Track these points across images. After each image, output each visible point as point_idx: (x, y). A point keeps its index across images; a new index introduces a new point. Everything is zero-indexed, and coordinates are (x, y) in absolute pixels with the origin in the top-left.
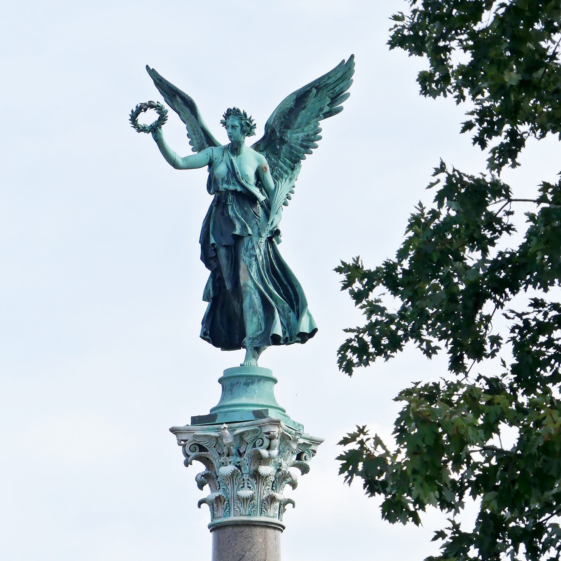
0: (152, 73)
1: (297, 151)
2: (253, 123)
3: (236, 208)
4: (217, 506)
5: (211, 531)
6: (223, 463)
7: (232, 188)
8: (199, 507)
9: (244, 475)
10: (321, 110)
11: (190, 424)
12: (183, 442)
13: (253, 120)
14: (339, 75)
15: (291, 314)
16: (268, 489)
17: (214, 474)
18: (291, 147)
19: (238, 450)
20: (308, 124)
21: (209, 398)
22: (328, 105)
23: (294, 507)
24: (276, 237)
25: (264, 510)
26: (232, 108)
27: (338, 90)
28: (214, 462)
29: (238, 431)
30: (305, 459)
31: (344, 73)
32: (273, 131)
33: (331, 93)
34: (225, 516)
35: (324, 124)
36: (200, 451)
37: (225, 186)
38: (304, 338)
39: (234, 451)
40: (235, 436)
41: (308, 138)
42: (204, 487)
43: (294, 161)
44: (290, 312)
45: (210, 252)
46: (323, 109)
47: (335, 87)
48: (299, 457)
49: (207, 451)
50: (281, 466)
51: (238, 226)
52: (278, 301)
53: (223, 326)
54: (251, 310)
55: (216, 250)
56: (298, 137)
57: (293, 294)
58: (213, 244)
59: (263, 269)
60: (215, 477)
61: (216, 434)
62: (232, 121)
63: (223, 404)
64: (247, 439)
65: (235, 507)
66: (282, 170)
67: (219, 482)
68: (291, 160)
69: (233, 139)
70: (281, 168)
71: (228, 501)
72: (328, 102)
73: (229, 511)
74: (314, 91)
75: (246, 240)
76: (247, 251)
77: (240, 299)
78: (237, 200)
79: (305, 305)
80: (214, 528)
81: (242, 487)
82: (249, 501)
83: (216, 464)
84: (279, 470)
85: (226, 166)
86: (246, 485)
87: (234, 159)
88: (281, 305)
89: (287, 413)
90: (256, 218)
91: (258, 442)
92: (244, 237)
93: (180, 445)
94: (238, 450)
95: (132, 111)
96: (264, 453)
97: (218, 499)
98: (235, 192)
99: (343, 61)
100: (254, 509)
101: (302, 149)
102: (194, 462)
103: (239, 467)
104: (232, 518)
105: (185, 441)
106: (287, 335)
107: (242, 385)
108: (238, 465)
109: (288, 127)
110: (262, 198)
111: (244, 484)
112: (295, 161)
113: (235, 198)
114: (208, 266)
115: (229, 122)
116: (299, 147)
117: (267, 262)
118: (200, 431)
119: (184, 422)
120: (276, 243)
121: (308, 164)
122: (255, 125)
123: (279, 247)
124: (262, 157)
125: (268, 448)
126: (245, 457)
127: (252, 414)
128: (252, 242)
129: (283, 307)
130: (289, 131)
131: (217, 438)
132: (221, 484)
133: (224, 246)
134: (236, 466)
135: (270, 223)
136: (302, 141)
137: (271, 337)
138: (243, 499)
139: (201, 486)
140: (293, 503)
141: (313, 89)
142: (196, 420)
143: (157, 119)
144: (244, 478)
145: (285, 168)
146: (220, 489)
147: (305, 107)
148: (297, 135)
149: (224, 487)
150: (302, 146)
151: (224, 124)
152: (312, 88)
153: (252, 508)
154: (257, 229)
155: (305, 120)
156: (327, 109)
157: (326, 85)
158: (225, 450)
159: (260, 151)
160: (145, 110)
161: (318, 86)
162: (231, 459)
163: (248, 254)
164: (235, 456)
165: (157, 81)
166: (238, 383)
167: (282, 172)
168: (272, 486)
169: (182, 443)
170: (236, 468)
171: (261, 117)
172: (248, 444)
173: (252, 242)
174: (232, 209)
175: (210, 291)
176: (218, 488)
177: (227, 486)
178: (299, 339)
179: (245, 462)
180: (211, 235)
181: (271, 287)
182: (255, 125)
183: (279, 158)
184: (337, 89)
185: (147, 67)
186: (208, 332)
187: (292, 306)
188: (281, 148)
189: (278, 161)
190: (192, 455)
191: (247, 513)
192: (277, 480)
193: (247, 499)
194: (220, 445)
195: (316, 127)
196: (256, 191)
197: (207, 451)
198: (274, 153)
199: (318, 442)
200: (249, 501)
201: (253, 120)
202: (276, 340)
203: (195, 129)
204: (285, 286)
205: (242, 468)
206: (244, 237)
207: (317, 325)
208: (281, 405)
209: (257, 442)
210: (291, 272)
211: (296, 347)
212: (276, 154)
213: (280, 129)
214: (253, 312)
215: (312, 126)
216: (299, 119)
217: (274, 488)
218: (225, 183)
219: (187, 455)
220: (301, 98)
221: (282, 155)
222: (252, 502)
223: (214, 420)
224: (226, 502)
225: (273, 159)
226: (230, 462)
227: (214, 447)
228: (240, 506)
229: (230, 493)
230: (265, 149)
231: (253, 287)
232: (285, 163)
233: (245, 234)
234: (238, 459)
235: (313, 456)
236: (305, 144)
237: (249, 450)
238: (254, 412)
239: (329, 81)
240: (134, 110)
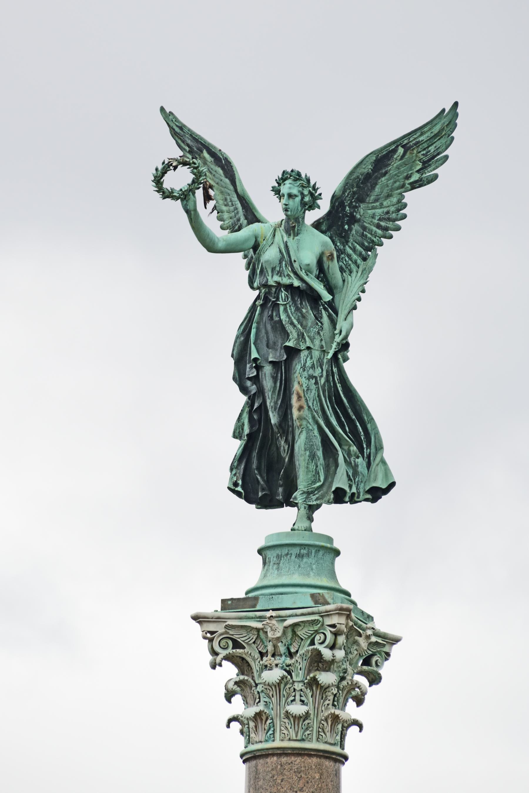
0: (168, 116)
1: (371, 234)
2: (319, 192)
3: (291, 309)
4: (256, 727)
5: (244, 762)
6: (266, 666)
7: (286, 281)
8: (228, 726)
9: (296, 684)
10: (408, 177)
11: (219, 610)
12: (208, 635)
13: (318, 188)
14: (436, 130)
15: (360, 460)
16: (328, 705)
17: (252, 681)
18: (364, 228)
19: (288, 649)
20: (389, 196)
21: (245, 575)
22: (418, 171)
23: (360, 731)
24: (342, 353)
25: (322, 734)
26: (289, 170)
27: (432, 151)
28: (252, 664)
29: (290, 621)
30: (377, 665)
31: (445, 124)
32: (342, 205)
33: (423, 155)
34: (266, 741)
35: (410, 197)
36: (233, 648)
37: (276, 278)
38: (376, 494)
39: (282, 649)
40: (286, 627)
41: (387, 216)
42: (233, 699)
43: (367, 247)
44: (358, 457)
45: (248, 369)
46: (410, 177)
47: (428, 147)
48: (367, 662)
49: (244, 648)
50: (345, 673)
51: (294, 334)
52: (343, 443)
53: (263, 472)
54: (308, 453)
55: (258, 368)
56: (374, 214)
57: (362, 433)
58: (256, 360)
59: (325, 397)
60: (254, 684)
61: (259, 625)
62: (290, 188)
63: (266, 583)
64: (301, 632)
65: (283, 728)
66: (351, 259)
67: (258, 692)
68: (362, 245)
69: (289, 213)
70: (349, 256)
71: (272, 719)
72: (418, 167)
73: (273, 734)
74: (401, 150)
75: (304, 354)
76: (304, 370)
77: (290, 438)
78: (293, 299)
79: (379, 448)
80: (248, 758)
81: (292, 701)
82: (302, 720)
83: (255, 666)
84: (343, 679)
85: (278, 250)
86: (298, 698)
87: (292, 243)
88: (346, 448)
89: (353, 598)
90: (317, 324)
91: (318, 638)
92: (300, 351)
93: (205, 638)
94: (288, 649)
95: (157, 169)
96: (327, 654)
97: (258, 716)
98: (290, 287)
99: (443, 110)
100: (308, 732)
101: (379, 232)
102: (224, 663)
103: (289, 673)
104: (277, 744)
105: (212, 633)
106: (354, 490)
107: (293, 557)
108: (288, 669)
109: (361, 200)
110: (327, 297)
111: (295, 696)
112: (370, 247)
113: (289, 296)
114: (244, 390)
115: (285, 189)
116: (374, 229)
117: (330, 387)
118: (233, 618)
119: (211, 606)
120: (341, 360)
121: (386, 251)
122: (320, 194)
123: (346, 366)
124: (326, 239)
125: (332, 647)
126: (297, 657)
127: (309, 599)
128: (311, 358)
129: (349, 451)
130: (362, 205)
131: (258, 630)
132: (262, 695)
133: (271, 362)
134: (285, 670)
135: (337, 332)
136: (380, 220)
137: (334, 492)
138: (295, 717)
139: (229, 696)
140: (361, 727)
141: (400, 148)
142: (226, 604)
143: (190, 182)
144: (296, 687)
145: (355, 257)
146: (259, 702)
147: (386, 173)
148: (373, 211)
149: (267, 700)
150: (378, 226)
151: (277, 191)
152: (397, 146)
153: (305, 731)
154: (319, 340)
155: (385, 191)
156: (415, 177)
157: (418, 142)
158: (270, 648)
159: (323, 232)
160: (175, 168)
161: (406, 144)
162: (279, 660)
163: (305, 374)
164: (284, 657)
165: (177, 130)
166: (287, 555)
167: (350, 262)
168: (334, 701)
169: (210, 637)
170: (286, 674)
171: (329, 183)
172: (302, 639)
173: (311, 358)
174: (285, 310)
175: (243, 424)
176: (257, 700)
177: (270, 698)
178: (369, 496)
179: (297, 665)
180: (253, 346)
181: (334, 422)
182: (320, 194)
183: (347, 242)
184: (432, 149)
185: (162, 109)
186: (240, 482)
187: (361, 449)
188: (350, 229)
189: (344, 246)
190: (223, 653)
191: (299, 738)
192: (340, 692)
193: (300, 717)
194: (262, 641)
195: (399, 201)
196: (319, 287)
197: (244, 648)
198: (340, 236)
199: (396, 640)
200: (302, 720)
201: (318, 188)
202: (339, 497)
203: (228, 198)
204: (353, 421)
205: (293, 674)
206: (300, 351)
207: (396, 478)
208: (344, 586)
209: (317, 637)
210: (362, 401)
211: (364, 507)
212: (344, 237)
213: (351, 202)
214: (309, 456)
215: (394, 200)
216: (377, 189)
217: (336, 703)
218: (277, 274)
219: (214, 653)
220: (381, 160)
221: (351, 240)
222: (307, 722)
223: (254, 606)
224: (269, 721)
225: (338, 244)
226: (277, 665)
227: (254, 643)
228: (289, 727)
229: (275, 708)
230: (329, 229)
231: (311, 420)
232: (354, 250)
233: (303, 347)
234: (288, 661)
235: (386, 659)
236: (383, 224)
237: (305, 648)
238: (313, 596)
239: (421, 139)
240: (160, 167)
